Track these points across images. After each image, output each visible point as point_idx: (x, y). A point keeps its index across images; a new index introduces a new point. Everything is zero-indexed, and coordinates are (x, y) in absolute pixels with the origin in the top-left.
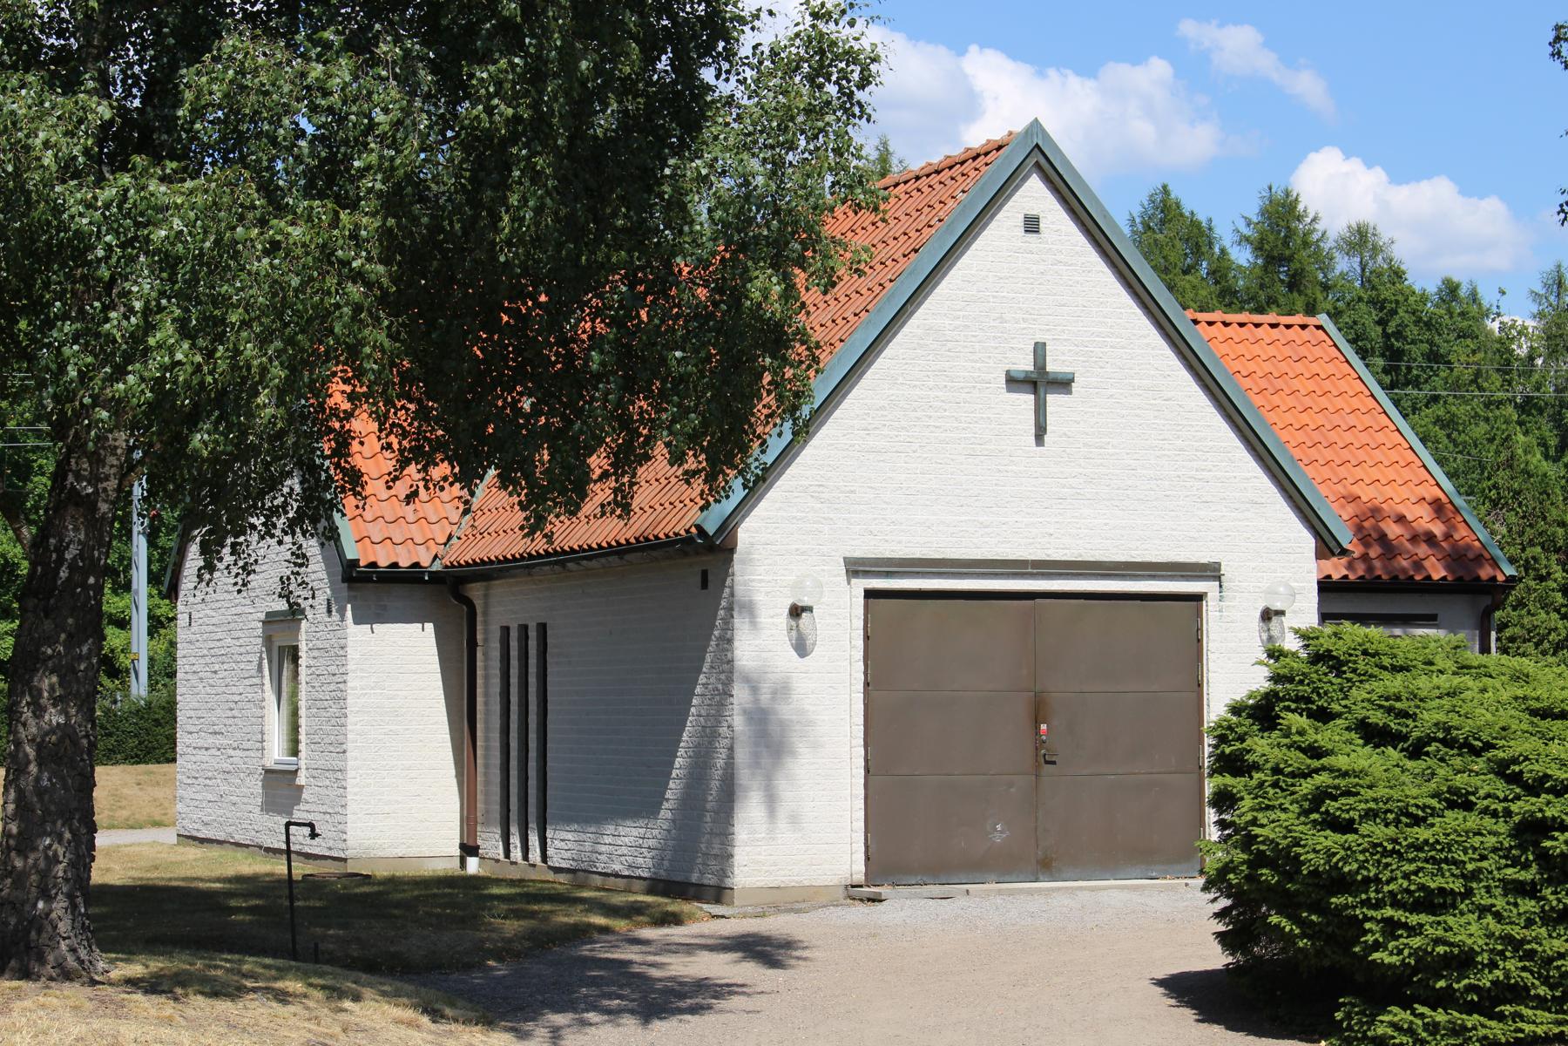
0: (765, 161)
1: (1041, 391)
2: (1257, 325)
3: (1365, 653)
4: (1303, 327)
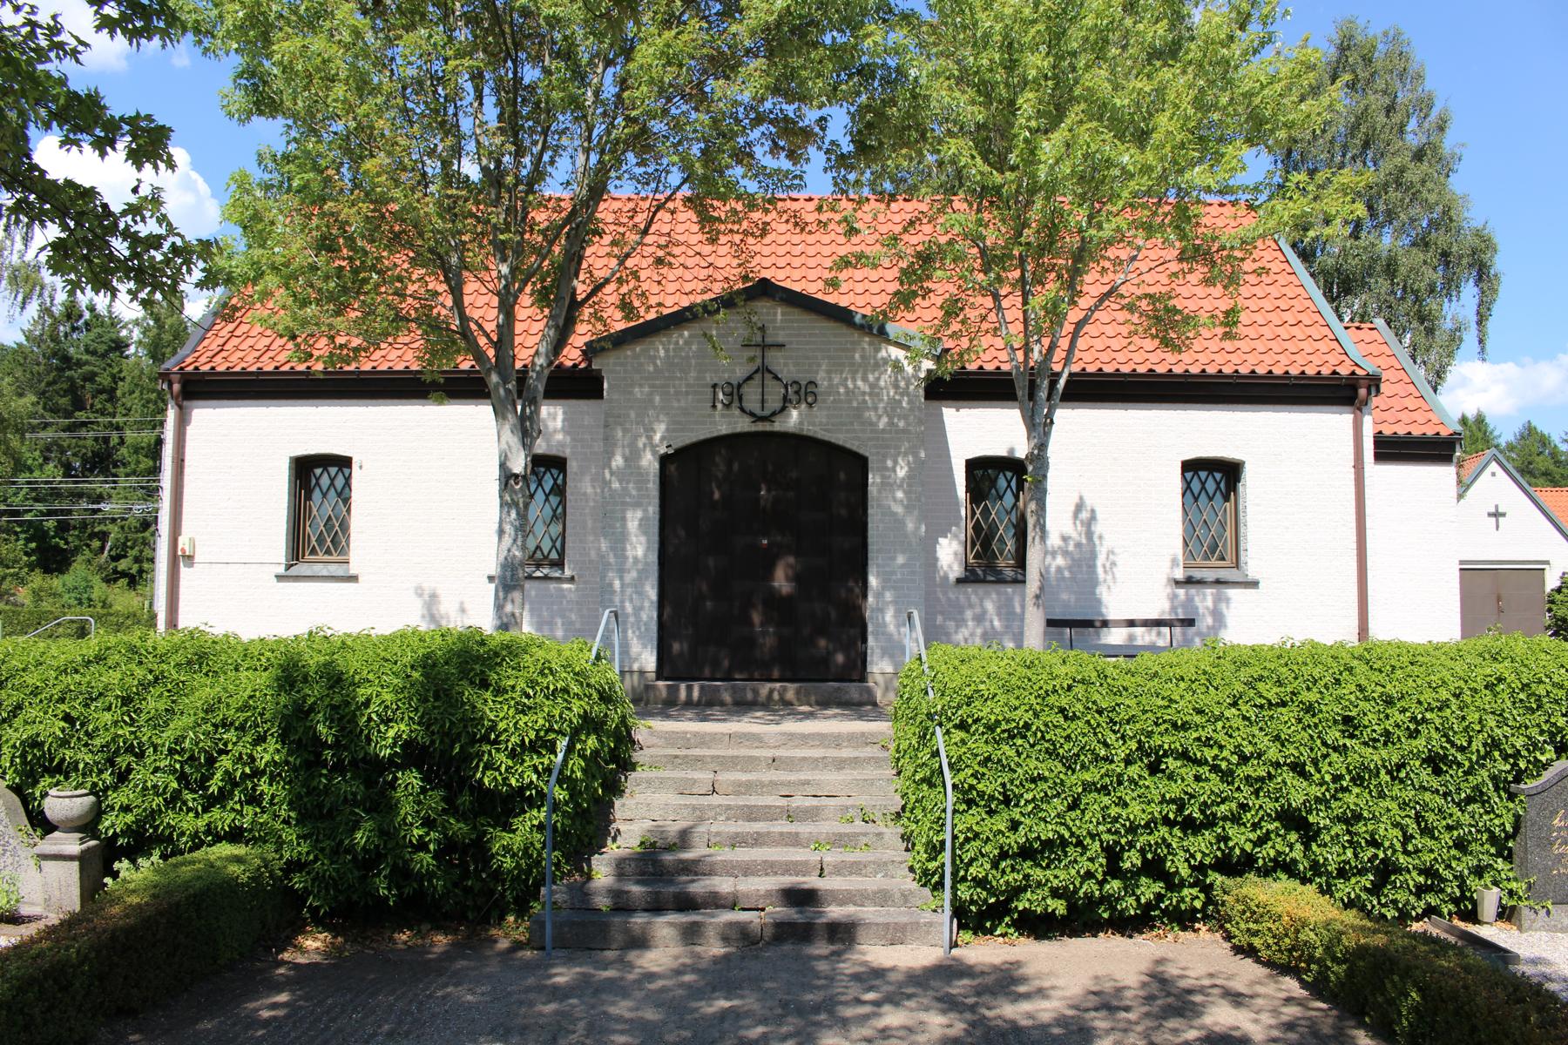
0: (787, 221)
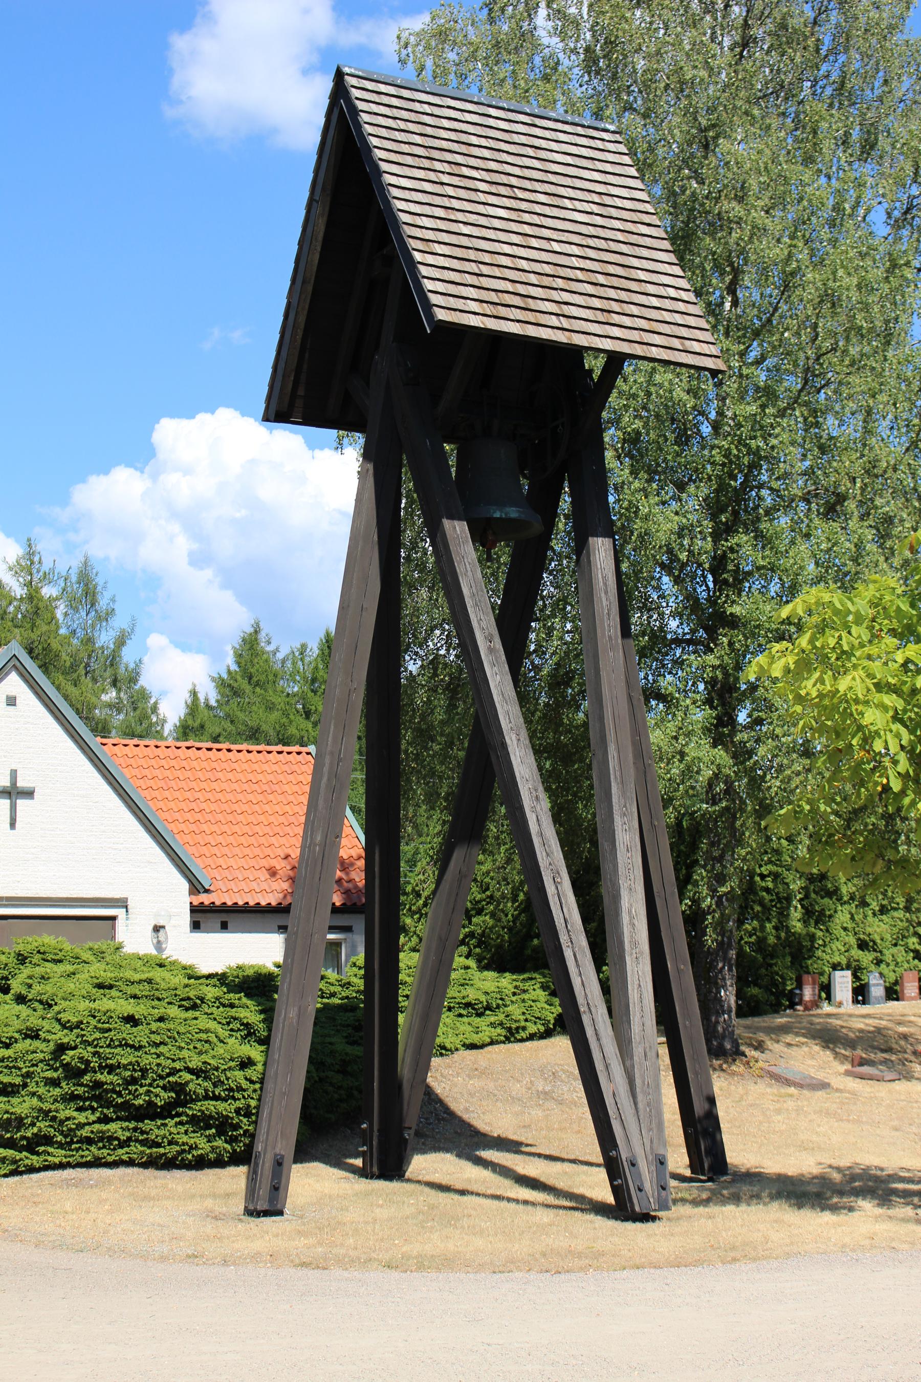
1: (14, 798)
2: (269, 752)
3: (39, 952)
4: (299, 753)
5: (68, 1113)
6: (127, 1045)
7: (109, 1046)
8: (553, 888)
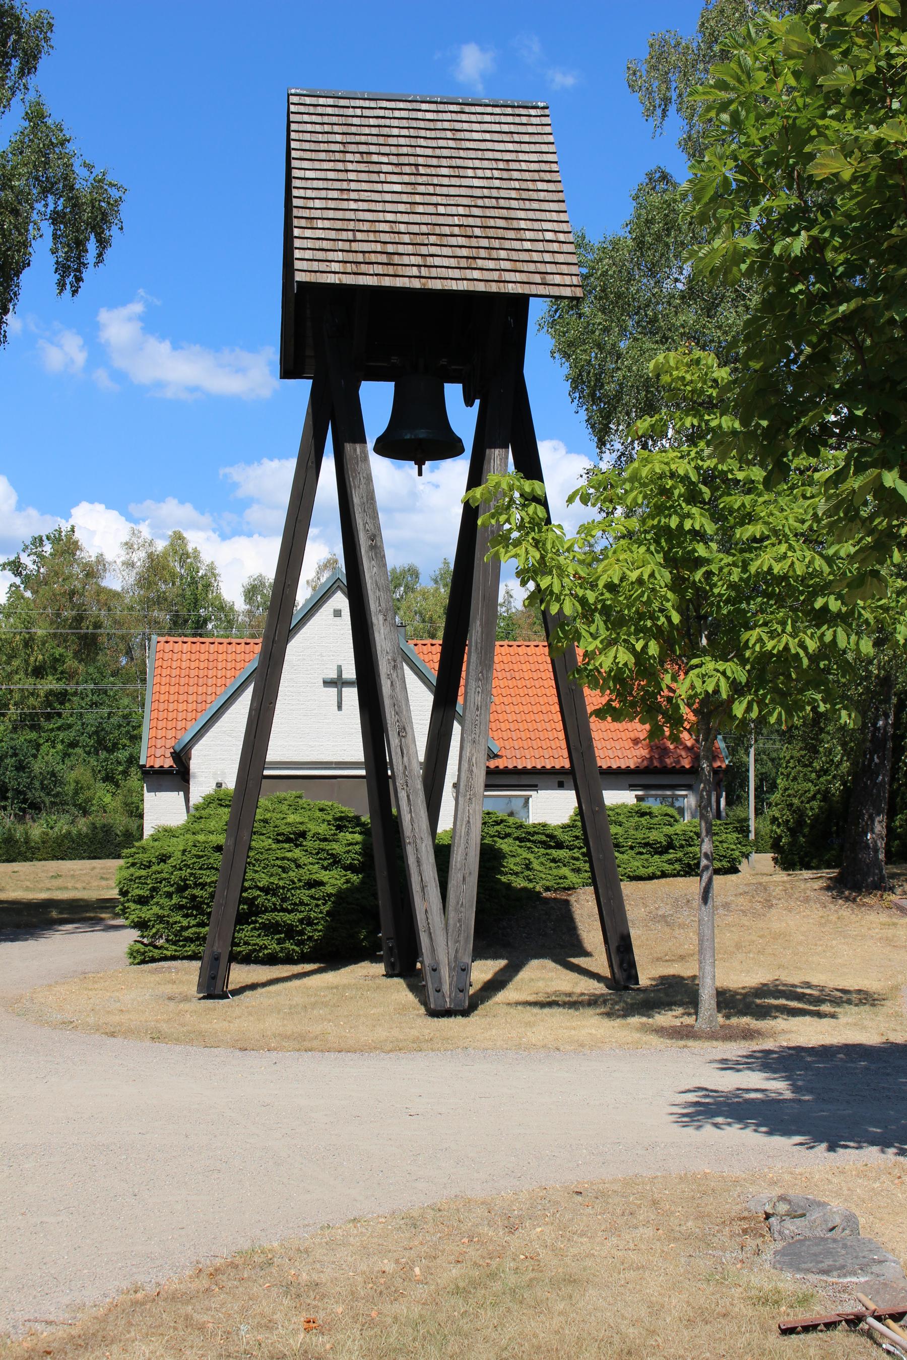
5: (179, 918)
6: (212, 868)
7: (200, 869)
8: (397, 741)
